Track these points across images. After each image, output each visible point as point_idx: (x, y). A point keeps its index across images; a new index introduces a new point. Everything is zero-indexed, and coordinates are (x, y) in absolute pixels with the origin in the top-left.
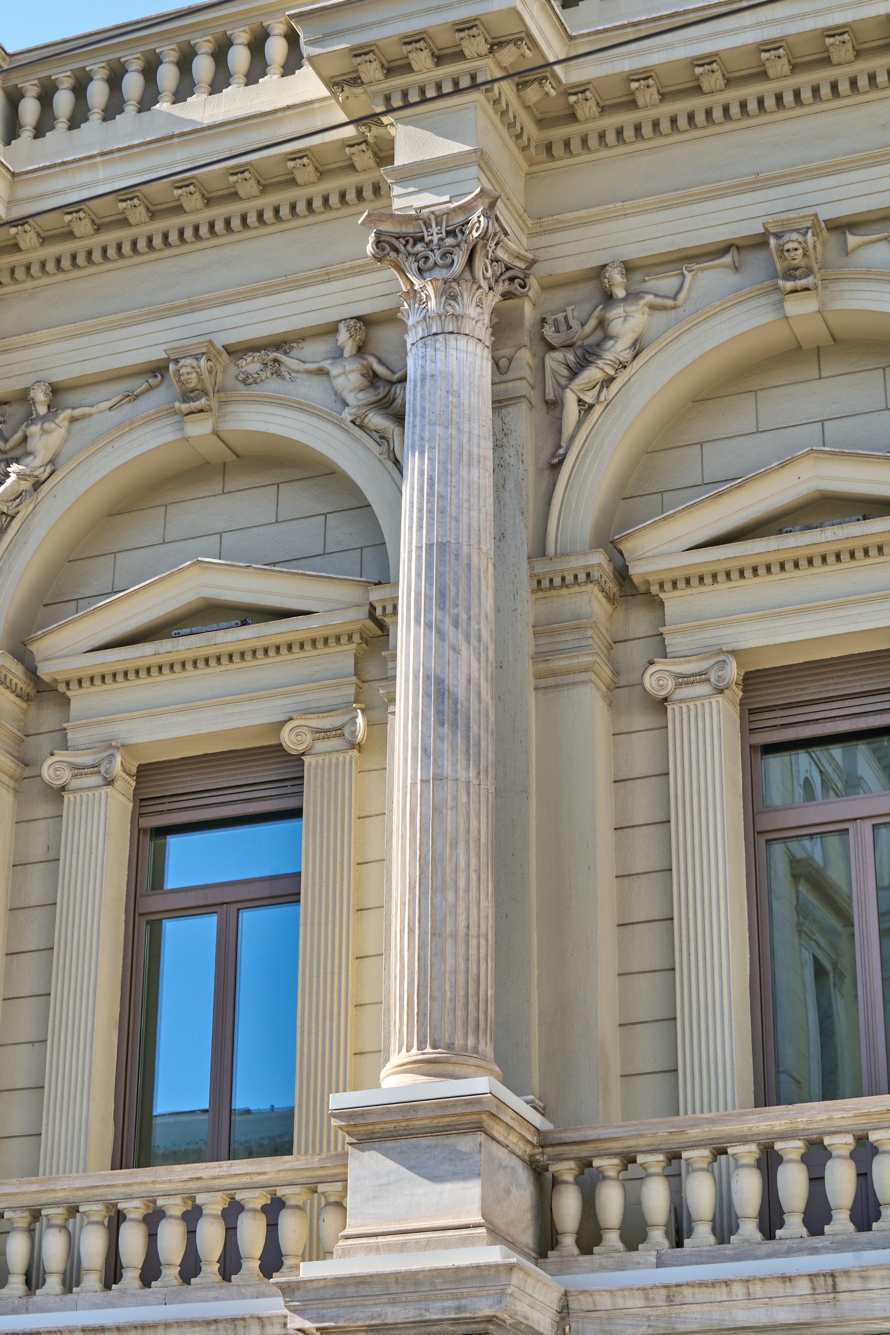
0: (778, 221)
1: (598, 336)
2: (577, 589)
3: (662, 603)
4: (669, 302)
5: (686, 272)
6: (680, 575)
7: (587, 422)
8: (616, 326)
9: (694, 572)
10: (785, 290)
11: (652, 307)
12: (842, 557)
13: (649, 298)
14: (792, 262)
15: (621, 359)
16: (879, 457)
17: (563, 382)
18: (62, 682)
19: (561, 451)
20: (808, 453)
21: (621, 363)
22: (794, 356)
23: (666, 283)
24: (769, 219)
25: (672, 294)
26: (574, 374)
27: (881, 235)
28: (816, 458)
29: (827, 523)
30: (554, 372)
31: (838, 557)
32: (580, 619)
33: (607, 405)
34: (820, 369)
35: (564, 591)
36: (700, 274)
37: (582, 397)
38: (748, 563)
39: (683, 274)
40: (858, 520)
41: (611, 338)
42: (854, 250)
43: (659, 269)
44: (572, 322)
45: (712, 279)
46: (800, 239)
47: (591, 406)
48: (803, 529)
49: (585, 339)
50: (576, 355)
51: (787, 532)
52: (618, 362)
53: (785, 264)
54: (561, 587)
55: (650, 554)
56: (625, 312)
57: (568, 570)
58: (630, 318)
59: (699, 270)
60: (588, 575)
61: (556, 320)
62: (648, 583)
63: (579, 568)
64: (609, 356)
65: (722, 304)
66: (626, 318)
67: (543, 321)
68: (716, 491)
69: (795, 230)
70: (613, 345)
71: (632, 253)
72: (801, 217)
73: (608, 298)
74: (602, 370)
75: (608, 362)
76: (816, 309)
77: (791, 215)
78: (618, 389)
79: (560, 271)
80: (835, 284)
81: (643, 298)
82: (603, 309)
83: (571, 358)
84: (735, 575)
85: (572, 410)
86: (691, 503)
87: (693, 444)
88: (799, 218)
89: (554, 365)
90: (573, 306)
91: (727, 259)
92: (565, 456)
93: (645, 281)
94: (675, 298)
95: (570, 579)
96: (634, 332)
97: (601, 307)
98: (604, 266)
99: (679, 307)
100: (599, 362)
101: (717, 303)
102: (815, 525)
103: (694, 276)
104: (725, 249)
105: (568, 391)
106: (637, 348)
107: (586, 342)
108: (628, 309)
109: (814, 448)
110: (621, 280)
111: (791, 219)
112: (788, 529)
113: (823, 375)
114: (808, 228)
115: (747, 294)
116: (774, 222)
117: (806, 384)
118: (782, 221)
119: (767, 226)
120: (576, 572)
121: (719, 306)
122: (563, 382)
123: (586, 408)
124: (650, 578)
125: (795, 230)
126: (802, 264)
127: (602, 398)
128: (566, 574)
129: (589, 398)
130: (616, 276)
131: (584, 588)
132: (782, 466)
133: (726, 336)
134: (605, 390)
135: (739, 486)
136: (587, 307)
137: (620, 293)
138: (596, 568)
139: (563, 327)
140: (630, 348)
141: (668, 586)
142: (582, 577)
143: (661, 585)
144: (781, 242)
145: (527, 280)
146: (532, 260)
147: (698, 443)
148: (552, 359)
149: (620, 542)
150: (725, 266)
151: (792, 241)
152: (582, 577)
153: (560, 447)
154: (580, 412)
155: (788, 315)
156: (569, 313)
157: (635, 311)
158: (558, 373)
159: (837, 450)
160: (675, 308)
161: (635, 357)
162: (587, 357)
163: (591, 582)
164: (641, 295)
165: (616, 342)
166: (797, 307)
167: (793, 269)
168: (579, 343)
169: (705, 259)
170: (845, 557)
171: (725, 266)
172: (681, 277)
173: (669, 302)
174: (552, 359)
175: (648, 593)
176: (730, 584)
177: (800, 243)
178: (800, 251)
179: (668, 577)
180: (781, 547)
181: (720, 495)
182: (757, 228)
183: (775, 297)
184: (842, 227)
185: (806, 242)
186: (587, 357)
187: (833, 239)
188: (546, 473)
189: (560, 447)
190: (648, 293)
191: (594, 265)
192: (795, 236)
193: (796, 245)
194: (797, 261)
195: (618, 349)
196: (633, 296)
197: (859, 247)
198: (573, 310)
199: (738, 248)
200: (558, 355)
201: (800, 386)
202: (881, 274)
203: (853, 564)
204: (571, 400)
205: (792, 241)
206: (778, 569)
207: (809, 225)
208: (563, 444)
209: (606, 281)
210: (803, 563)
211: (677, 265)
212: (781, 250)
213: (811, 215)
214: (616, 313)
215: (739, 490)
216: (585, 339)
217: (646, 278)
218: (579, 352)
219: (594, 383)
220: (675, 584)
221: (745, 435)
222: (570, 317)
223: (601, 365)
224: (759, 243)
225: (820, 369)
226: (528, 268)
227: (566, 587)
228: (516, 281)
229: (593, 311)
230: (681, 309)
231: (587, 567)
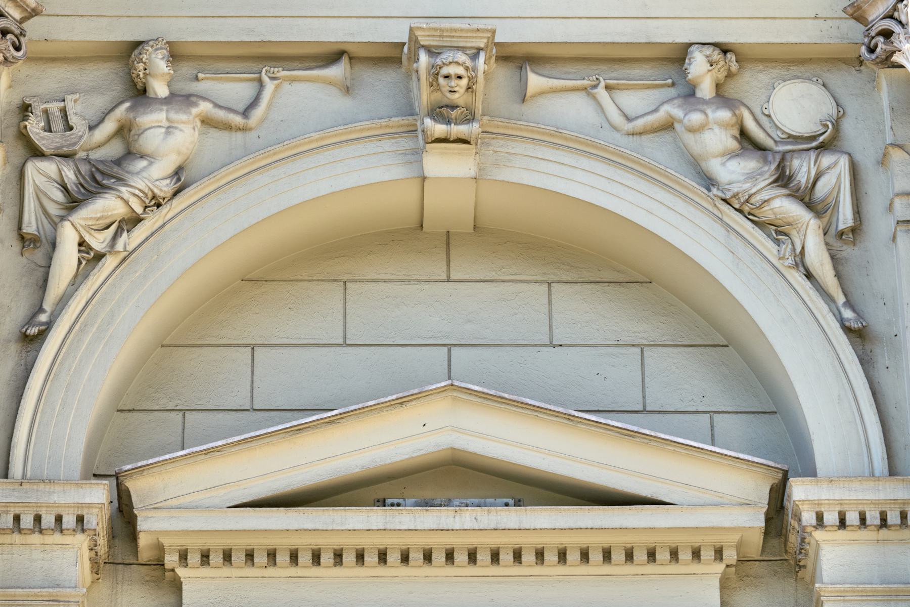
0: (435, 30)
1: (115, 149)
2: (57, 538)
3: (177, 586)
4: (237, 120)
5: (265, 78)
6: (216, 544)
7: (91, 279)
8: (151, 140)
9: (239, 544)
10: (432, 135)
11: (207, 122)
12: (479, 557)
13: (205, 107)
14: (449, 95)
15: (157, 192)
16: (557, 414)
17: (54, 210)
18: (239, 550)
19: (43, 318)
20: (444, 390)
21: (154, 197)
22: (414, 237)
23: (236, 90)
24: (423, 24)
25: (241, 107)
26: (73, 203)
27: (579, 83)
28: (455, 399)
29: (458, 501)
30: (39, 193)
31: (472, 557)
32: (58, 586)
33: (124, 259)
34: (448, 265)
35: (36, 538)
36: (286, 86)
37: (87, 238)
38: (328, 543)
39: (260, 81)
40: (507, 505)
41: (142, 156)
42: (533, 96)
43: (221, 65)
44: (73, 120)
45: (303, 98)
46: (469, 63)
47: (99, 257)
48: (417, 504)
49: (91, 149)
50: (78, 172)
51: (392, 505)
52: (150, 195)
53: (437, 96)
54: (32, 531)
55: (175, 502)
56: (168, 119)
57: (48, 506)
58: (177, 132)
59: (286, 79)
60: (80, 519)
61: (46, 112)
62: (160, 549)
63: (67, 505)
64: (140, 183)
65: (322, 139)
66: (169, 129)
67: (25, 109)
68: (295, 423)
69: (458, 48)
70: (145, 168)
71: (186, 31)
72: (473, 31)
73: (139, 93)
74: (127, 202)
75: (137, 192)
76: (472, 173)
77: (457, 24)
78: (143, 237)
79: (63, 37)
80: (501, 142)
81: (195, 105)
82: (129, 109)
83: (70, 175)
84: (305, 558)
85: (67, 257)
86: (253, 434)
87: (239, 345)
88: (468, 31)
89: (41, 181)
90: (77, 96)
91: (336, 71)
92: (49, 326)
93: (197, 79)
94: (245, 113)
95: (48, 520)
96: (179, 153)
97: (127, 105)
98: (138, 44)
99: (250, 129)
100: (123, 189)
101: (315, 135)
102: (438, 502)
103: (277, 87)
104: (334, 56)
105: (67, 224)
106: (181, 180)
107: (95, 155)
108: (174, 116)
109: (456, 383)
110: (166, 70)
111: (455, 30)
112: (396, 501)
113: (453, 276)
114: (479, 49)
115: (362, 130)
116: (430, 29)
117: (426, 286)
118: (442, 30)
119: (418, 33)
120: (844, 508)
121: (317, 140)
122: (54, 210)
123: (91, 257)
124: (166, 542)
125: (458, 48)
126: (461, 102)
127: (120, 246)
128: (43, 512)
129: (98, 242)
130: (159, 63)
131: (68, 539)
132: (402, 402)
133: (324, 188)
134: (125, 234)
135: (330, 422)
136: (100, 102)
137: (160, 89)
138: (95, 511)
139: (58, 125)
140: (171, 176)
141: (194, 558)
142: (69, 521)
143: (183, 557)
144: (439, 61)
145: (22, 39)
146: (34, 10)
147: (246, 346)
148: (39, 171)
149: (131, 476)
150: (330, 82)
151: (457, 63)
152: (69, 521)
153: (41, 310)
154: (80, 263)
155: (426, 174)
156: (69, 105)
157: (184, 123)
158: (46, 195)
159: (492, 392)
160: (243, 129)
161: (176, 194)
162: (99, 177)
163: (83, 531)
164: (194, 99)
165: (151, 163)
166: (443, 164)
167: (447, 106)
168: (81, 154)
169: (295, 65)
170: (371, 558)
171: (330, 82)
172: (256, 84)
173: (237, 120)
174: (39, 171)
175: (160, 563)
176: (293, 571)
177: (467, 69)
178: (464, 82)
179: (195, 544)
180: (389, 527)
181: (299, 430)
182: (398, 33)
183: (406, 144)
184: (519, 59)
185: (475, 69)
186: (97, 180)
187: (504, 75)
188: (14, 348)
189: (41, 310)
190: (204, 99)
191: (119, 39)
192: (461, 57)
193: (461, 71)
194: (456, 96)
195: (152, 176)
196: (180, 99)
197: (542, 93)
198: (75, 101)
199: (351, 58)
200: (49, 167)
201: (414, 287)
202: (576, 140)
203: (495, 570)
204: (68, 237)
205: (457, 63)
206: (556, 558)
207: (482, 46)
208: (48, 306)
209: (141, 66)
210: (484, 557)
211: (255, 66)
212: (435, 73)
213: (487, 31)
214: (152, 119)
215: (329, 427)
216: (91, 149)
217: (200, 75)
218: (84, 169)
219: (108, 221)
220: (205, 557)
221: (324, 345)
222: (70, 113)
223: (126, 196)
224: (390, 57)
225: (448, 265)
226: (22, 21)
227: (41, 531)
228: (9, 36)
229: (112, 109)
230: (254, 134)
231: (81, 505)
